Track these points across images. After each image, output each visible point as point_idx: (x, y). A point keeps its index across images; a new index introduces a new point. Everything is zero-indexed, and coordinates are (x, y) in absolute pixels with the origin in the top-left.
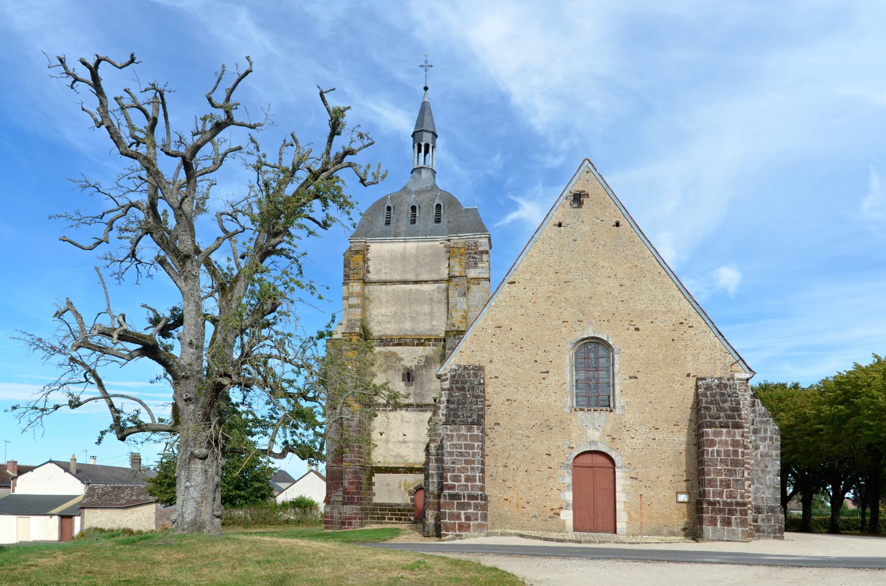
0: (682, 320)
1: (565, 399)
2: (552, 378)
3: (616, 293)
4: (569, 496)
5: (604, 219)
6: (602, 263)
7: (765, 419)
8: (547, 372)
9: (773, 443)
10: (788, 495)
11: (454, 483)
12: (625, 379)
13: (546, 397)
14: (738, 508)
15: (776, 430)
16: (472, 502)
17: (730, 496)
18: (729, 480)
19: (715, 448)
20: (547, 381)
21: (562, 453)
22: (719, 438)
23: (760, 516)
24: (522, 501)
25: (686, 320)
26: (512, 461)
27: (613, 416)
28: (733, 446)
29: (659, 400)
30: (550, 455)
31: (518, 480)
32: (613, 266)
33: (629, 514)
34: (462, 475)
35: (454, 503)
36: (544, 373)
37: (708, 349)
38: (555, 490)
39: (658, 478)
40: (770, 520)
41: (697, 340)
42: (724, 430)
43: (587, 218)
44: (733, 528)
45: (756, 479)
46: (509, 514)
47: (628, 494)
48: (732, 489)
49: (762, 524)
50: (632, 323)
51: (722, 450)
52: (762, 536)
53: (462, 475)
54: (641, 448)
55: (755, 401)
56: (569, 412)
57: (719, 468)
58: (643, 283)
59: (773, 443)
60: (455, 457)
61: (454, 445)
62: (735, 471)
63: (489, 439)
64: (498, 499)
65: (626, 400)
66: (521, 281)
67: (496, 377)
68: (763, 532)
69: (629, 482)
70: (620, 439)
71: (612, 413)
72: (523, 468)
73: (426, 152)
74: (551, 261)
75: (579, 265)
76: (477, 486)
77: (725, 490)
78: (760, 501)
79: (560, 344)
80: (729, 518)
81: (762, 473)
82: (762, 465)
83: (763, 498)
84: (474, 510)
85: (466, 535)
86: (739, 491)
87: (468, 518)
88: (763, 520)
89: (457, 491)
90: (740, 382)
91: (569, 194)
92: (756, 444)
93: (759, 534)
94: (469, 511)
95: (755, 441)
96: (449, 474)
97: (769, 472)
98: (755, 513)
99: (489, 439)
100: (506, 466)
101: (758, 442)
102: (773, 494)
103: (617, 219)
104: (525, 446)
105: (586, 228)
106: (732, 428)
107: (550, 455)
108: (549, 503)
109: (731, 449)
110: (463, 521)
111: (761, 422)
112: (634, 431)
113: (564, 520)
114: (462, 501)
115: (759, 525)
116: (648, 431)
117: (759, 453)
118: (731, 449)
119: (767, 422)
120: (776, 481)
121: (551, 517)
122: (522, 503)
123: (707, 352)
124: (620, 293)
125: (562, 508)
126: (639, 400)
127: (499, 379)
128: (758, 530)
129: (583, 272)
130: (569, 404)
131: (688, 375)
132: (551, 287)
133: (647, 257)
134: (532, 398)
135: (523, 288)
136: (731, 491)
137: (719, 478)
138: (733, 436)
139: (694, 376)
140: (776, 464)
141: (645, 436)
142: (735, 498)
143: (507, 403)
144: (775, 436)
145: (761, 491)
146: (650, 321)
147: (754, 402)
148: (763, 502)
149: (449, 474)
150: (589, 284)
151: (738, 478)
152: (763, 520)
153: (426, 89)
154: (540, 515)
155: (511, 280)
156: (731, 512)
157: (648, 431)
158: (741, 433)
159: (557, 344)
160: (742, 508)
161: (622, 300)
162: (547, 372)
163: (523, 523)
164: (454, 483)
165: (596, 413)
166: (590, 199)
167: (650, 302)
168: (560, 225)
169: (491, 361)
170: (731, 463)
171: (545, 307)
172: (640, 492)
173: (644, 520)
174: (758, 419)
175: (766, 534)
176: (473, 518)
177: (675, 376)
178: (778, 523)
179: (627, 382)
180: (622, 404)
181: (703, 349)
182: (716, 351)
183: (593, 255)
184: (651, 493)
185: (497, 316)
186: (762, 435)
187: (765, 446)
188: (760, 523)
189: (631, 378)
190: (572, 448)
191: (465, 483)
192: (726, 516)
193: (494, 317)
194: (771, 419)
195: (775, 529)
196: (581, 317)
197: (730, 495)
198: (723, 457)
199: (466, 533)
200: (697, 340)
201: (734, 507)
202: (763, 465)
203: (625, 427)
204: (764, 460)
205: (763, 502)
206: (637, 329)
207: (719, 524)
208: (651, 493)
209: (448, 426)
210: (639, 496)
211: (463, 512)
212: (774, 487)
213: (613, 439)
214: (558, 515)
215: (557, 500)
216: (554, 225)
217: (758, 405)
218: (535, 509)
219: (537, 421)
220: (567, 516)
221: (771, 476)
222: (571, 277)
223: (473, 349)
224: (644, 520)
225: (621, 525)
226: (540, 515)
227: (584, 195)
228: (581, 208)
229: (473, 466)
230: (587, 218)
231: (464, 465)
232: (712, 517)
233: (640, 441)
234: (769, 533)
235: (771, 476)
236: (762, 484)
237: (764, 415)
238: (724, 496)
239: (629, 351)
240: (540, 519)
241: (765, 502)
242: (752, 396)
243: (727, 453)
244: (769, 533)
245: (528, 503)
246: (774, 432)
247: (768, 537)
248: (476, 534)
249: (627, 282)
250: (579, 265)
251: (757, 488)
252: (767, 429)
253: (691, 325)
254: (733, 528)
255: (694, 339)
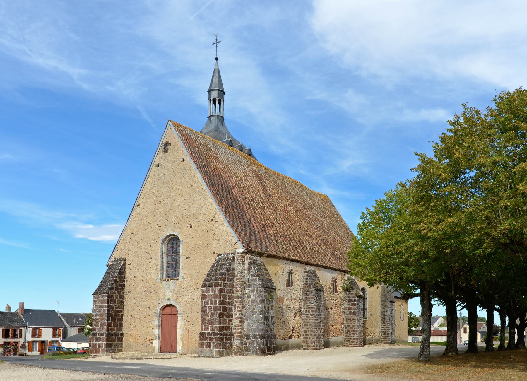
0: (213, 218)
1: (158, 273)
2: (153, 262)
3: (182, 205)
4: (157, 332)
5: (177, 157)
6: (176, 187)
7: (254, 278)
8: (151, 259)
9: (258, 293)
10: (519, 318)
11: (96, 327)
12: (184, 259)
13: (150, 274)
14: (214, 337)
15: (260, 284)
16: (101, 337)
17: (212, 330)
18: (212, 319)
19: (206, 300)
20: (151, 264)
21: (155, 307)
22: (208, 294)
23: (249, 340)
24: (137, 336)
25: (214, 217)
26: (134, 313)
27: (178, 283)
28: (214, 298)
29: (199, 271)
30: (150, 308)
31: (136, 323)
32: (181, 188)
33: (183, 341)
34: (99, 322)
35: (94, 338)
36: (150, 259)
37: (224, 235)
38: (151, 328)
39: (197, 319)
40: (254, 343)
41: (219, 230)
42: (211, 288)
43: (170, 159)
44: (211, 349)
45: (249, 317)
46: (132, 343)
47: (183, 329)
48: (213, 325)
49: (249, 346)
50: (189, 223)
51: (209, 301)
52: (249, 354)
53: (99, 322)
54: (189, 301)
55: (250, 266)
56: (159, 282)
57: (207, 312)
58: (194, 196)
59: (258, 293)
60: (97, 313)
61: (96, 306)
62: (215, 313)
63: (126, 300)
64: (128, 335)
65: (185, 272)
66: (142, 204)
67: (130, 264)
68: (250, 351)
69: (184, 322)
70: (180, 297)
71: (178, 281)
72: (138, 317)
73: (219, 103)
74: (154, 189)
75: (166, 190)
76: (105, 328)
77: (210, 326)
78: (250, 331)
79: (157, 241)
80: (210, 343)
81: (252, 313)
82: (252, 308)
83: (252, 329)
84: (102, 341)
85: (98, 355)
86: (216, 326)
87: (99, 346)
88: (250, 343)
89: (97, 332)
90: (238, 255)
91: (162, 145)
92: (249, 295)
93: (248, 352)
94: (100, 342)
95: (249, 292)
96: (94, 322)
97: (255, 312)
98: (246, 339)
99: (126, 300)
100: (132, 316)
101: (251, 293)
102: (258, 327)
103: (184, 157)
104: (140, 303)
105: (169, 166)
106: (214, 287)
107: (150, 308)
108: (148, 336)
109: (213, 300)
110: (97, 348)
111: (253, 280)
112: (187, 291)
113: (154, 346)
114: (98, 337)
115: (248, 347)
116: (193, 290)
117: (251, 300)
118: (213, 300)
119: (254, 280)
120: (259, 318)
121: (149, 344)
122: (137, 337)
123: (223, 237)
124: (184, 204)
125: (153, 339)
126: (191, 272)
127: (131, 265)
128: (247, 349)
129: (168, 194)
130: (159, 277)
131: (214, 253)
132: (154, 205)
133: (197, 179)
134: (144, 275)
135: (142, 208)
136: (213, 326)
137: (207, 318)
138: (214, 292)
139: (217, 253)
140: (259, 307)
141: (192, 293)
142: (214, 330)
143: (134, 279)
144: (259, 289)
145: (251, 325)
146: (197, 221)
147: (250, 267)
148: (252, 332)
149: (94, 322)
150: (170, 201)
151: (216, 318)
152: (250, 343)
153: (217, 59)
154: (144, 343)
155: (138, 204)
156: (211, 339)
157: (193, 290)
158: (219, 289)
159: (156, 241)
160: (216, 336)
161: (185, 209)
162: (151, 259)
163: (137, 348)
164: (96, 327)
165: (171, 282)
166: (171, 146)
167: (198, 208)
168: (158, 165)
169: (128, 255)
170: (213, 309)
171: (151, 219)
172: (188, 328)
173: (189, 345)
174: (251, 278)
175: (251, 352)
176: (101, 346)
177: (207, 255)
178: (258, 345)
179: (185, 260)
180: (183, 275)
181: (222, 236)
182: (228, 236)
183: (172, 182)
184: (193, 329)
185: (132, 227)
186: (252, 288)
187: (253, 296)
188: (248, 345)
189: (187, 258)
190: (160, 303)
191: (100, 327)
192: (208, 342)
193: (131, 228)
194: (258, 278)
195: (257, 349)
196: (167, 222)
197: (212, 328)
198: (210, 306)
199: (98, 354)
200: (219, 230)
201: (212, 336)
202: (252, 308)
203: (183, 289)
204: (253, 305)
205: (252, 332)
206: (191, 227)
207: (205, 346)
208: (193, 329)
209: (95, 295)
210: (187, 330)
211: (97, 343)
212: (258, 322)
213: (178, 296)
214: (152, 343)
215: (152, 335)
216: (156, 166)
217: (252, 269)
218: (142, 340)
219: (146, 288)
220: (156, 344)
221: (257, 315)
222: (162, 198)
223: (122, 248)
224: (189, 345)
225: (179, 348)
226: (144, 343)
227: (168, 144)
228: (167, 153)
229: (103, 317)
230: (170, 159)
231: (100, 317)
232: (202, 342)
233: (189, 297)
234: (253, 352)
235: (257, 315)
236: (252, 320)
237: (254, 275)
238: (209, 330)
239: (187, 241)
240: (144, 346)
241: (253, 332)
242: (249, 263)
243: (211, 302)
244: (253, 352)
245: (140, 336)
246: (259, 286)
247: (253, 354)
248: (102, 355)
249: (187, 197)
250: (166, 190)
251: (249, 323)
252: (255, 284)
253: (216, 220)
254: (211, 349)
255: (218, 229)
